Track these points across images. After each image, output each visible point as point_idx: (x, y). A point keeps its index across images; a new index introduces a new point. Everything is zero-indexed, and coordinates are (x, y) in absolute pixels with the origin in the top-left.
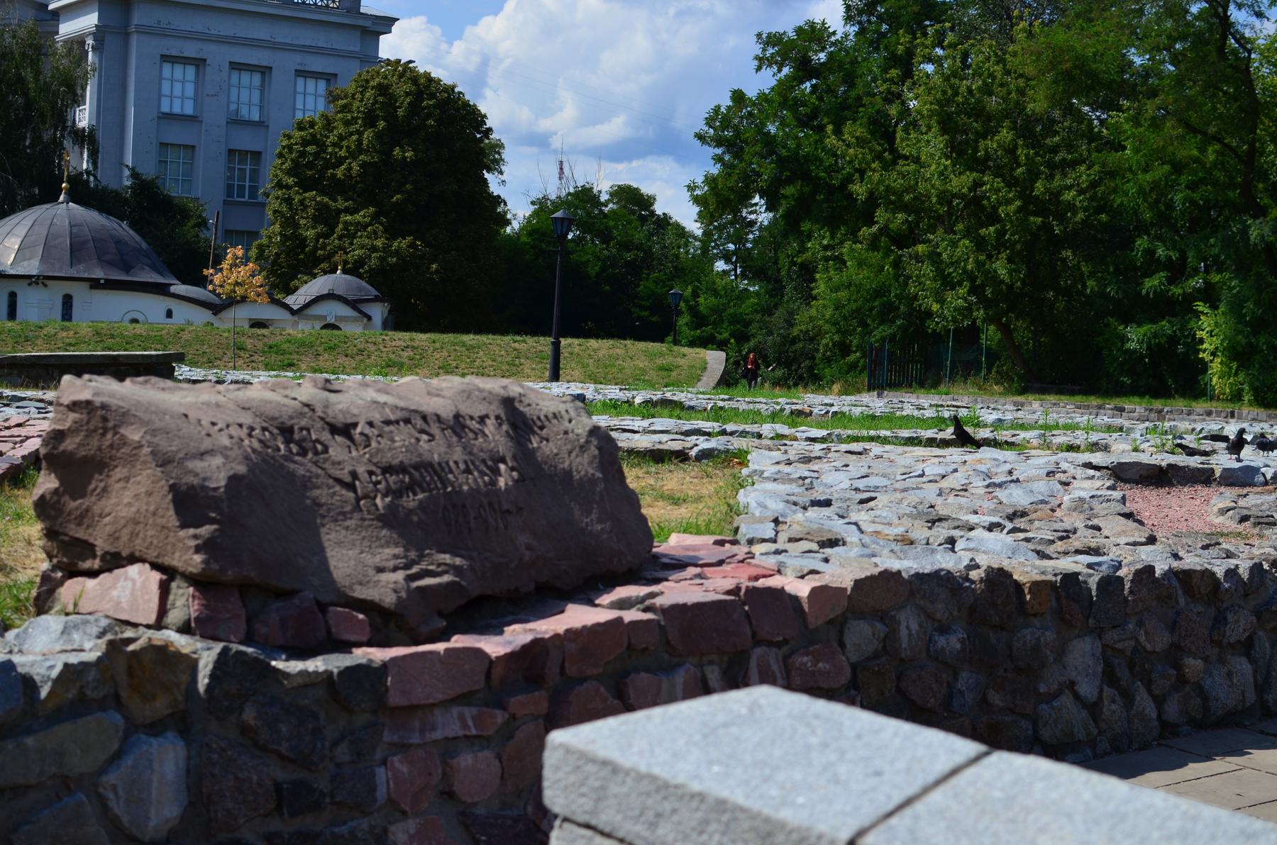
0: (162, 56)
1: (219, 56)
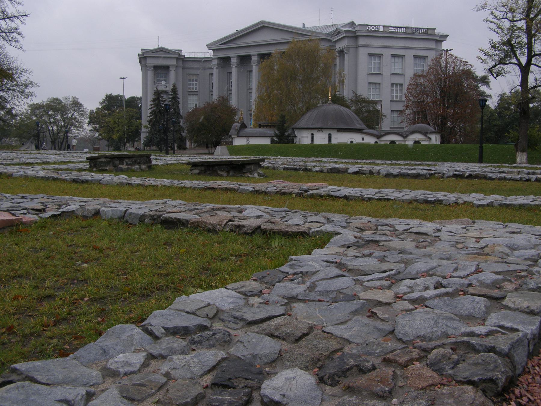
0: (368, 54)
1: (387, 53)
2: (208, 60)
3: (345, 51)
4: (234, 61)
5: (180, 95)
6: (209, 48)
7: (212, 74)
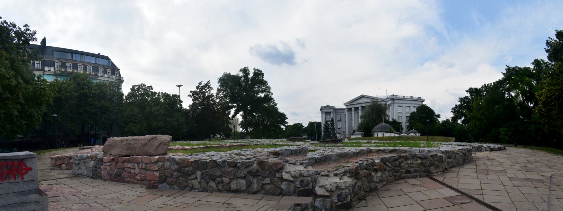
1: (404, 105)
2: (344, 109)
3: (390, 105)
4: (353, 109)
5: (335, 122)
6: (344, 105)
7: (345, 114)
